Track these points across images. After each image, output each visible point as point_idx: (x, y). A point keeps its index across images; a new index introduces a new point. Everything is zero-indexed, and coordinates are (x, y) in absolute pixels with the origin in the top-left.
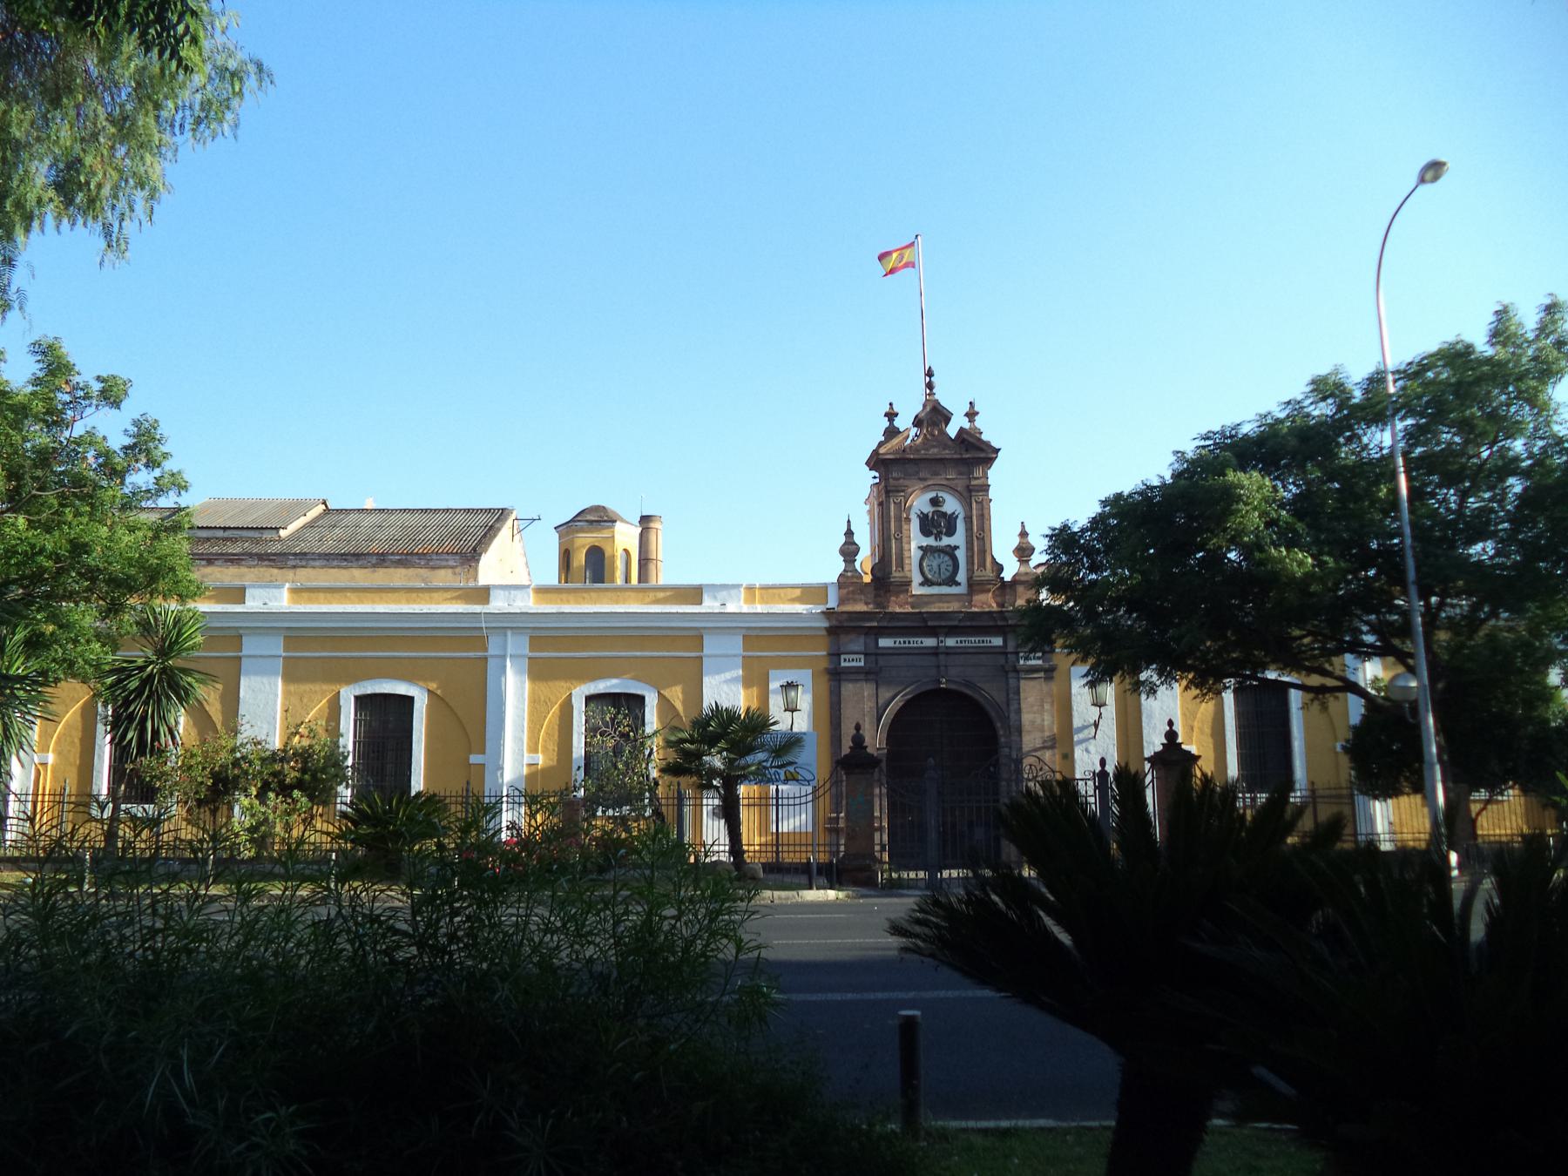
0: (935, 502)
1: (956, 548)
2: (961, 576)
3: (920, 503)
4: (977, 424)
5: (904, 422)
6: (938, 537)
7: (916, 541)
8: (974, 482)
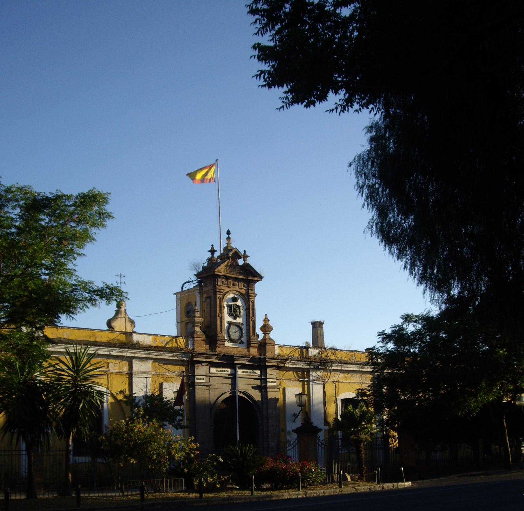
6: (235, 318)
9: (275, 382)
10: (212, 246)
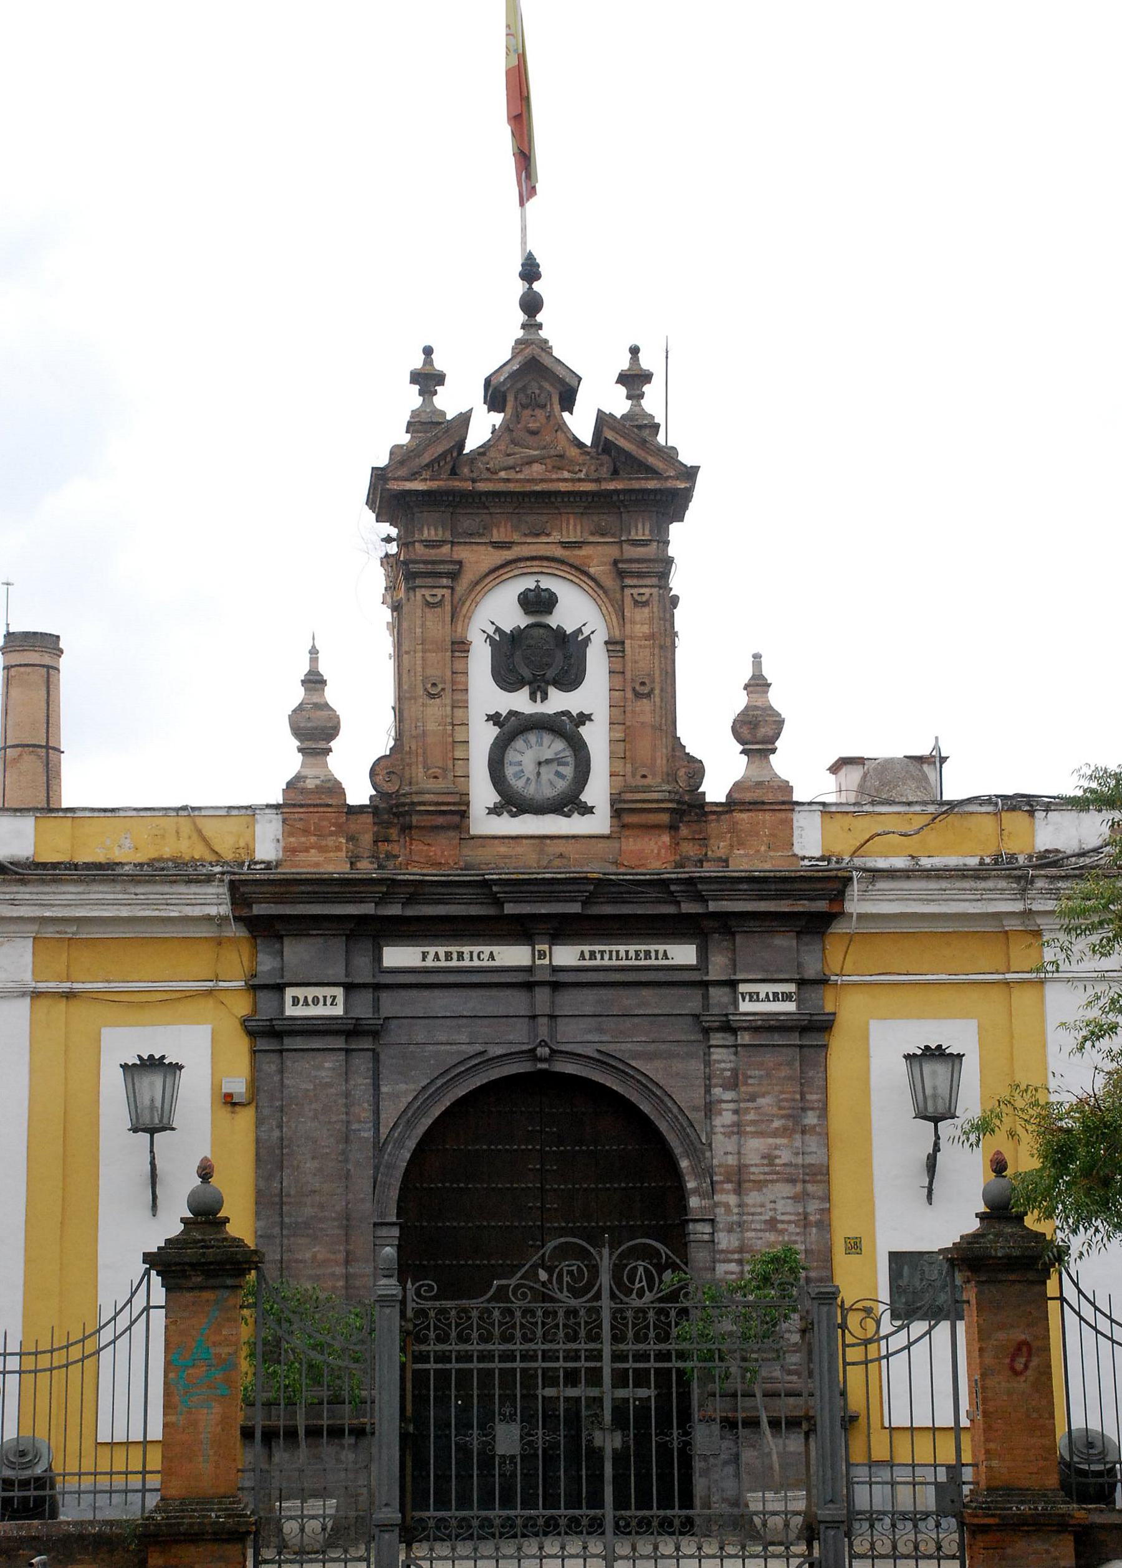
0: (538, 603)
1: (584, 718)
2: (598, 791)
3: (500, 609)
4: (652, 402)
5: (462, 395)
6: (539, 692)
7: (487, 695)
8: (631, 552)
9: (787, 997)
10: (428, 351)
